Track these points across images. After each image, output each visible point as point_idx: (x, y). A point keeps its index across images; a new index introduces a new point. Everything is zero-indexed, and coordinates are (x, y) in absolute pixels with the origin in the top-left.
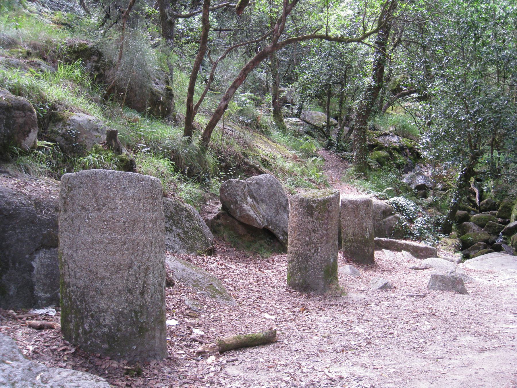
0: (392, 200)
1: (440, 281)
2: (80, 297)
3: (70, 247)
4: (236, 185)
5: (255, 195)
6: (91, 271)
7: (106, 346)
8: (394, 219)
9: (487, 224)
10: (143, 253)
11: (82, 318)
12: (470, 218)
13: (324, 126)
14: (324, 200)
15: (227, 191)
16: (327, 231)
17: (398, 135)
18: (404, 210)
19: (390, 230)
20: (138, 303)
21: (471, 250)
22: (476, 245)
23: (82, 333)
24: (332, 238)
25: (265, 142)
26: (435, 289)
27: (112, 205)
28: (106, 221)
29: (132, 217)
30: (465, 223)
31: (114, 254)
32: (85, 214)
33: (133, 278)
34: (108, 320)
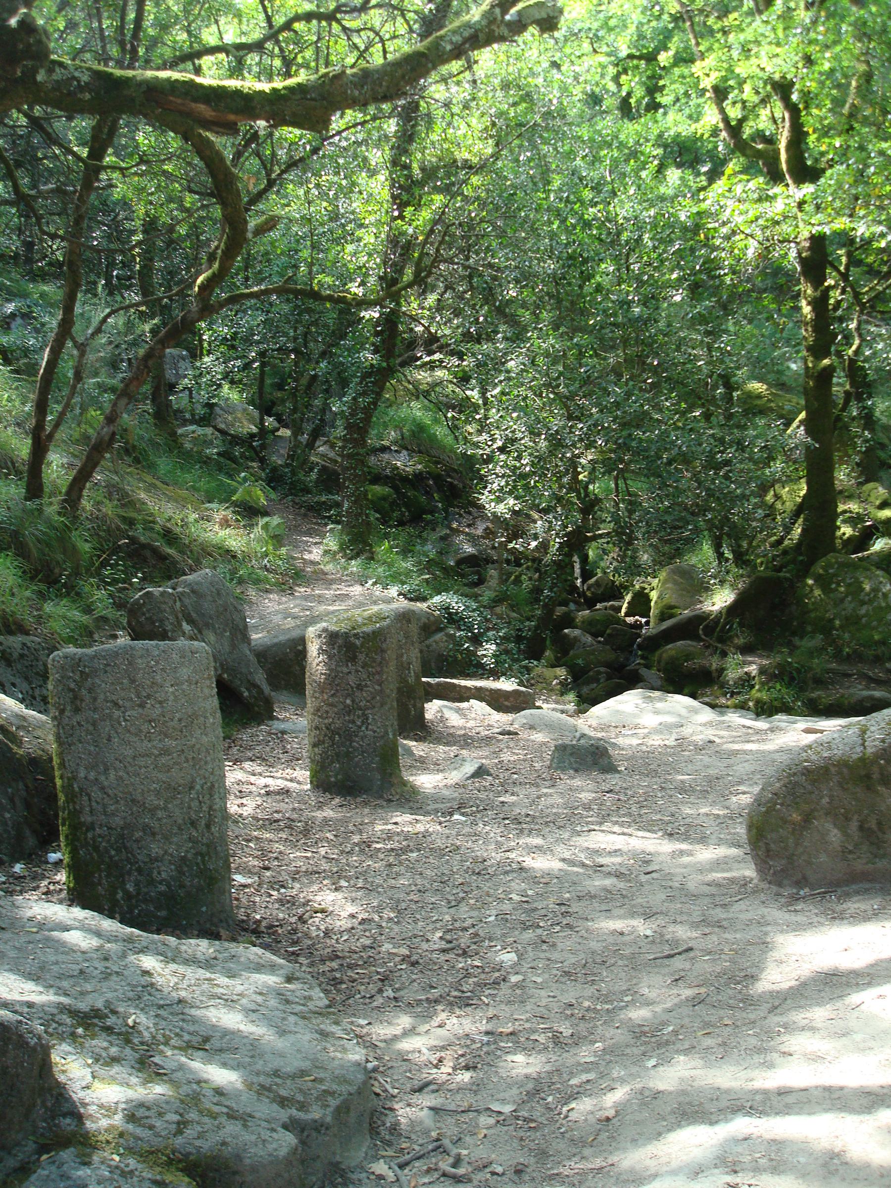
0: (437, 599)
1: (571, 754)
2: (116, 842)
3: (90, 767)
4: (162, 599)
5: (194, 615)
6: (133, 801)
7: (163, 913)
8: (445, 638)
9: (608, 631)
10: (206, 763)
11: (122, 876)
12: (573, 619)
13: (252, 436)
14: (374, 632)
15: (144, 614)
16: (380, 685)
17: (407, 449)
18: (462, 619)
19: (447, 661)
20: (205, 841)
21: (584, 684)
22: (591, 673)
23: (123, 898)
24: (388, 696)
25: (150, 485)
26: (563, 770)
27: (160, 696)
28: (154, 721)
29: (190, 711)
30: (566, 631)
31: (168, 771)
32: (117, 713)
33: (197, 803)
34: (165, 872)
